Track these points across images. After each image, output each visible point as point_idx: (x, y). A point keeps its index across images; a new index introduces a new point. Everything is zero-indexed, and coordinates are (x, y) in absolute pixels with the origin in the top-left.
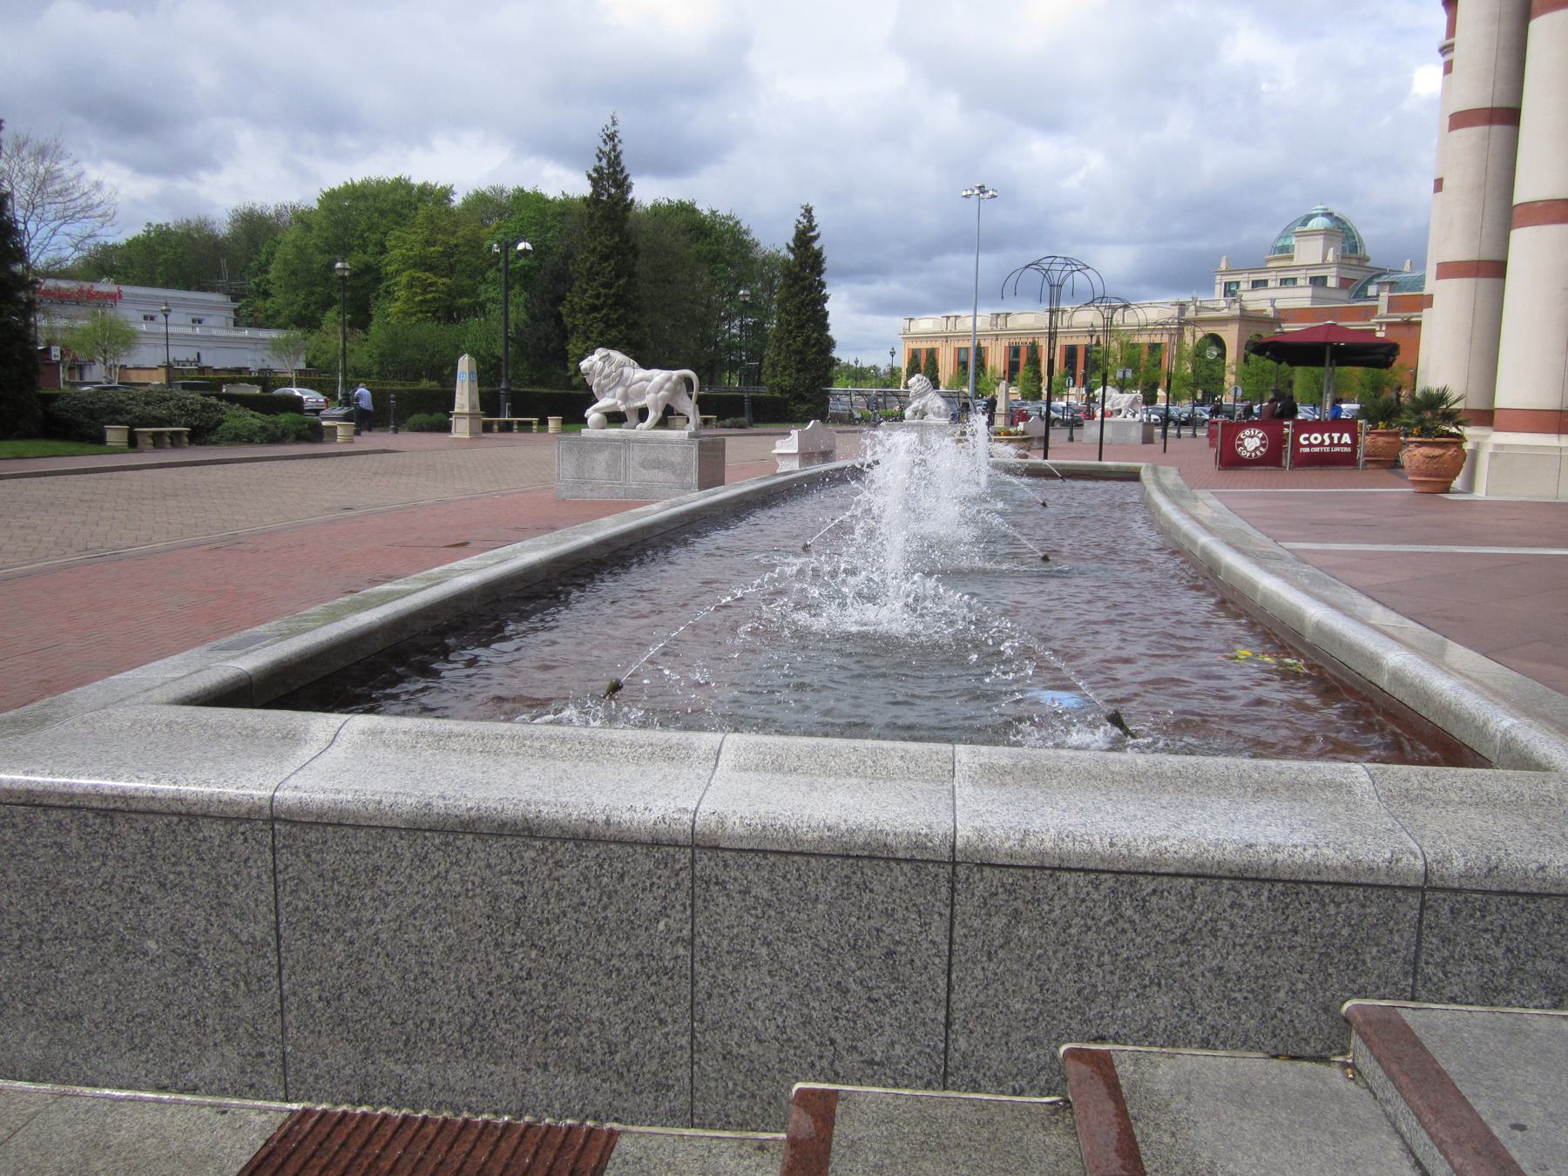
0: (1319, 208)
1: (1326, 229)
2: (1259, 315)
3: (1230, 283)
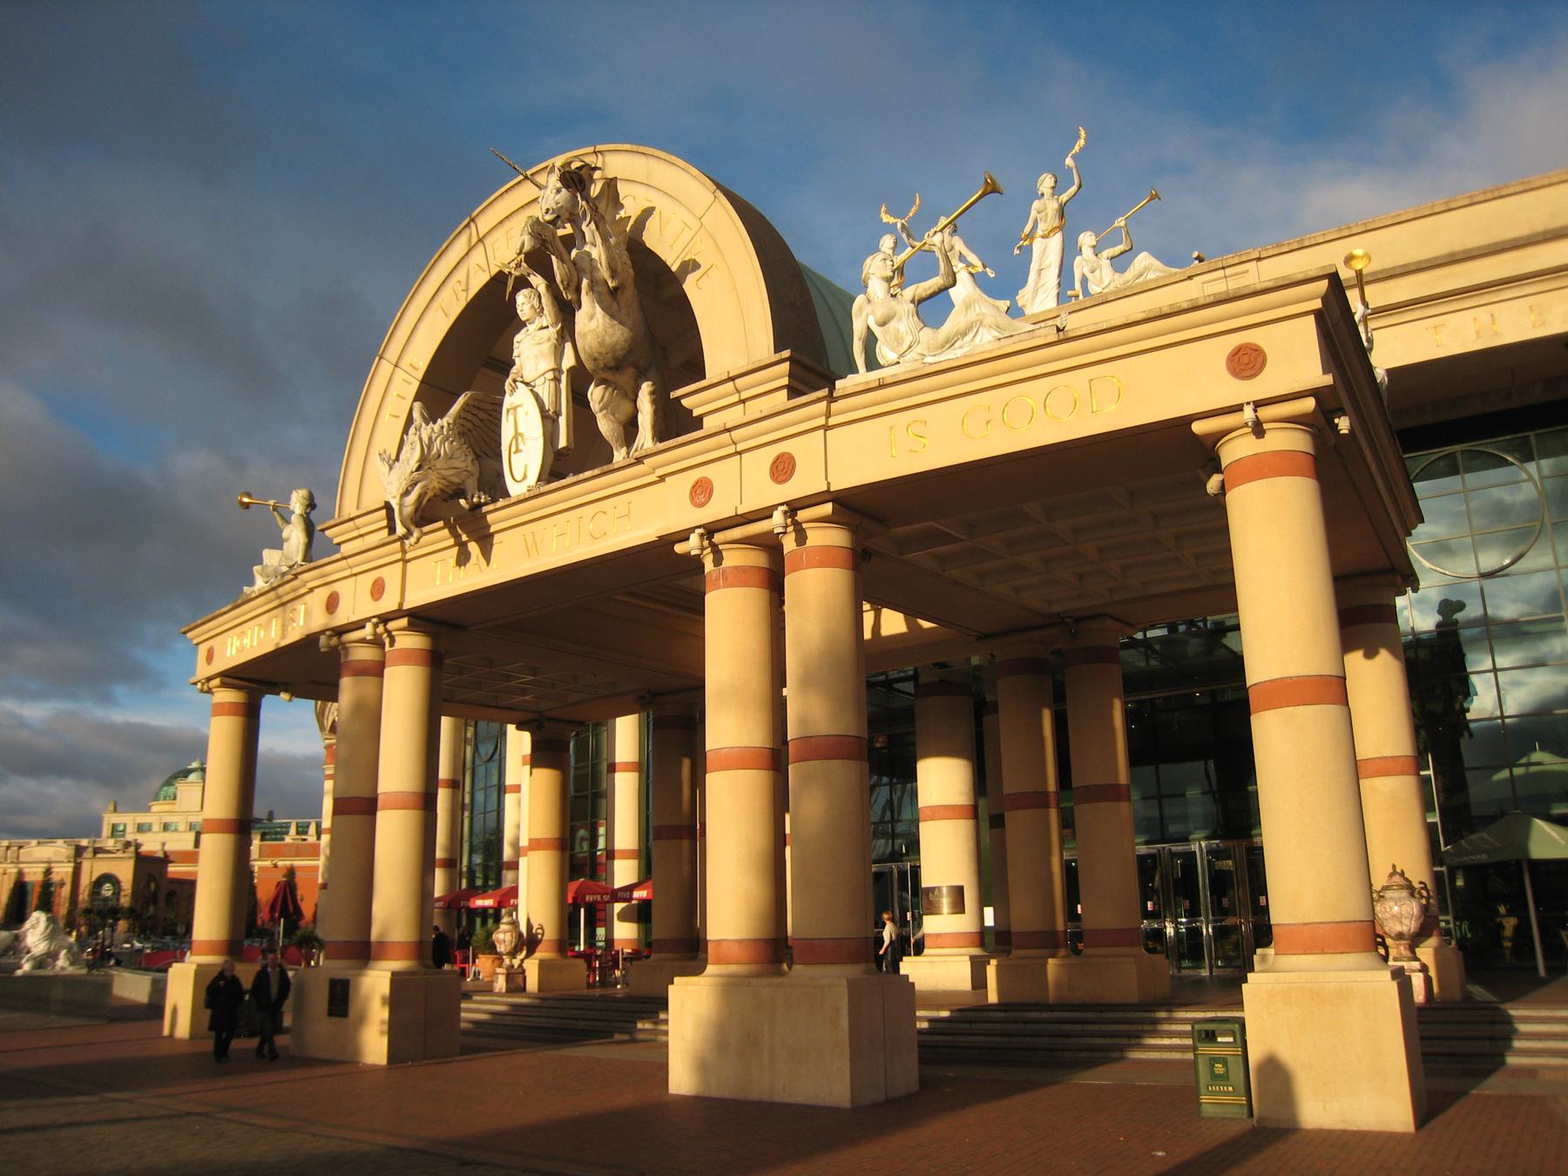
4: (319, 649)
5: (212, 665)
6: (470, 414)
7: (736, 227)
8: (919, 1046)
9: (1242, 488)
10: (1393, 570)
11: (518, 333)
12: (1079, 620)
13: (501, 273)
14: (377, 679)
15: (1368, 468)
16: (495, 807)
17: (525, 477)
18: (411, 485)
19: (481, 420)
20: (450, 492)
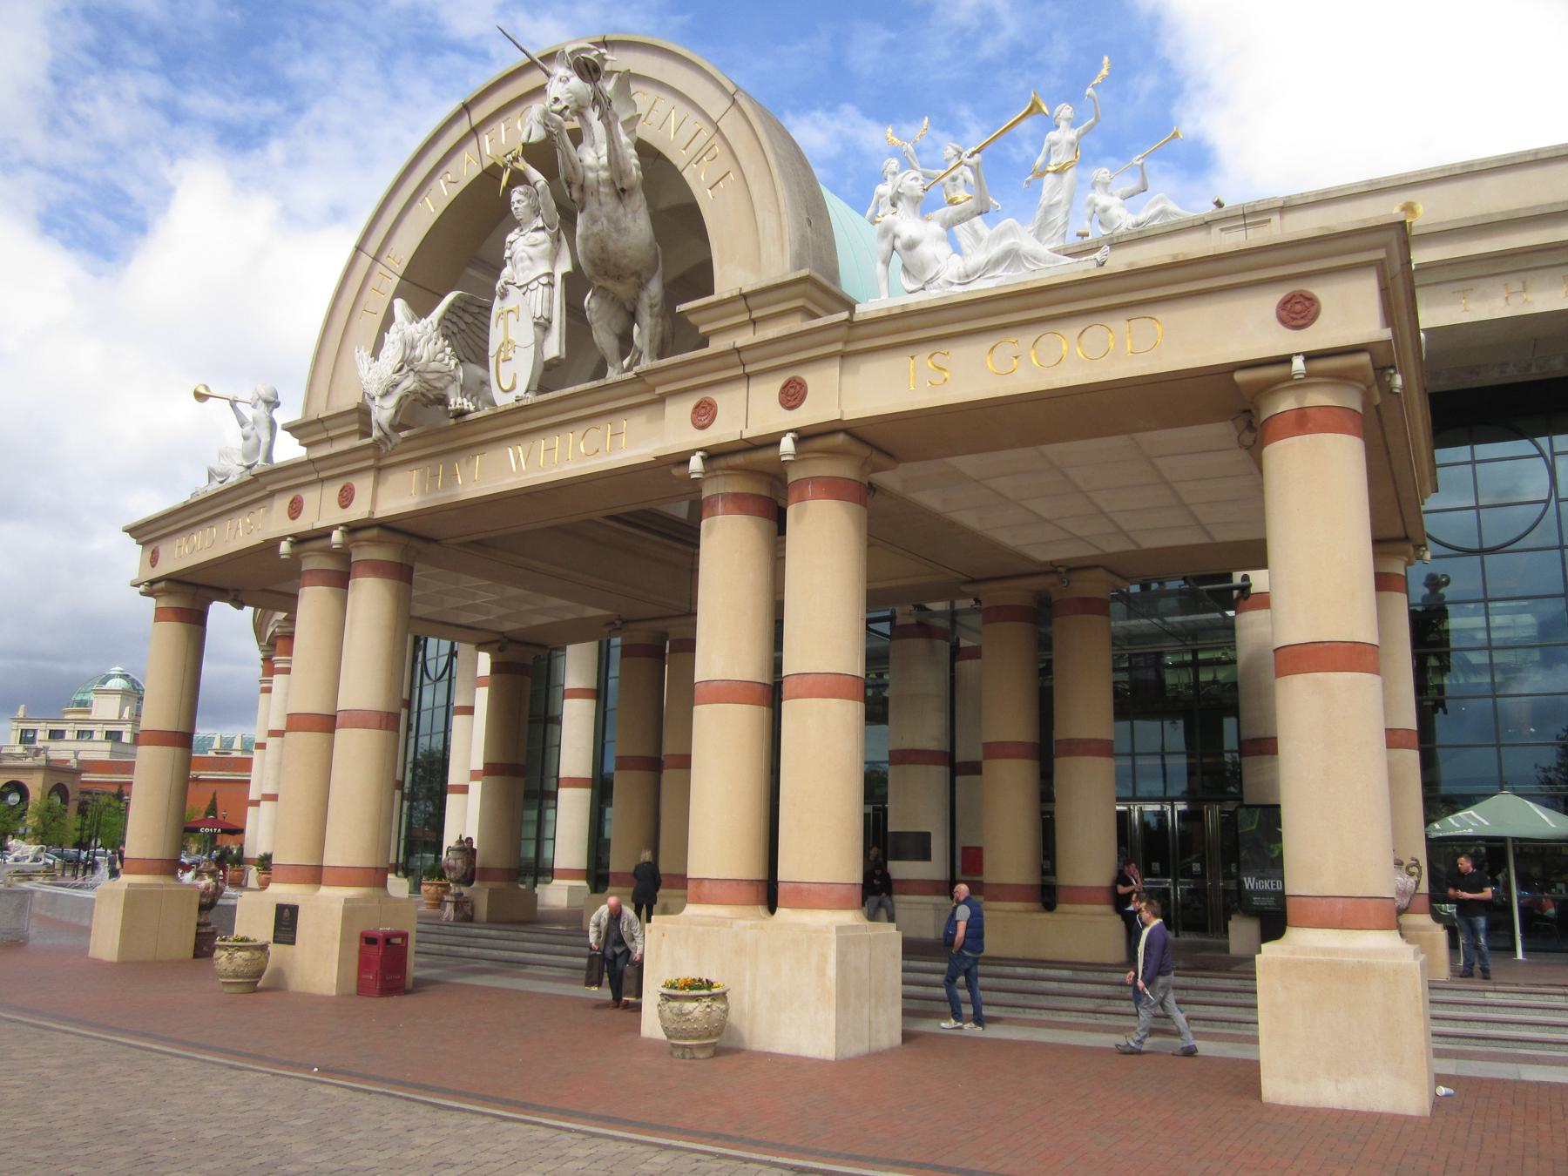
0: (116, 670)
1: (123, 690)
2: (63, 766)
3: (27, 730)
4: (280, 556)
5: (155, 568)
6: (455, 317)
7: (695, 156)
8: (903, 997)
9: (1282, 442)
10: (1406, 539)
11: (511, 232)
12: (1070, 570)
13: (495, 165)
14: (345, 590)
15: (1406, 429)
16: (442, 729)
17: (513, 388)
18: (392, 387)
19: (466, 323)
20: (432, 397)
